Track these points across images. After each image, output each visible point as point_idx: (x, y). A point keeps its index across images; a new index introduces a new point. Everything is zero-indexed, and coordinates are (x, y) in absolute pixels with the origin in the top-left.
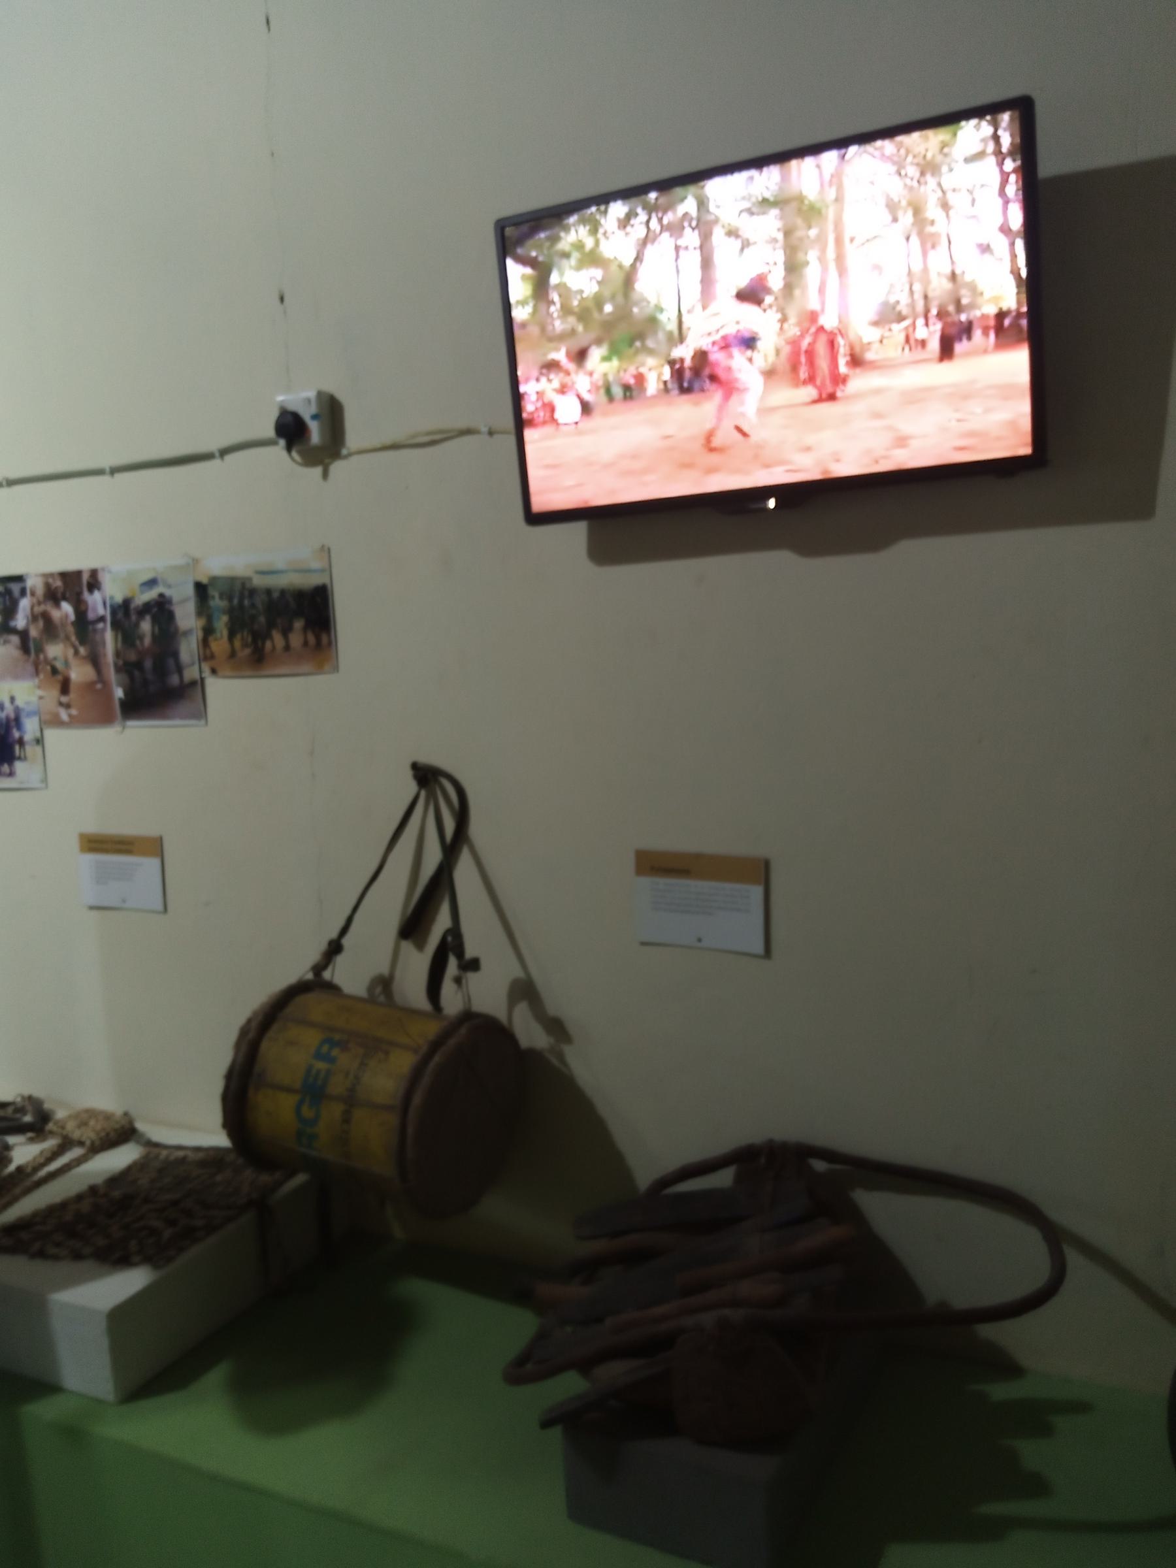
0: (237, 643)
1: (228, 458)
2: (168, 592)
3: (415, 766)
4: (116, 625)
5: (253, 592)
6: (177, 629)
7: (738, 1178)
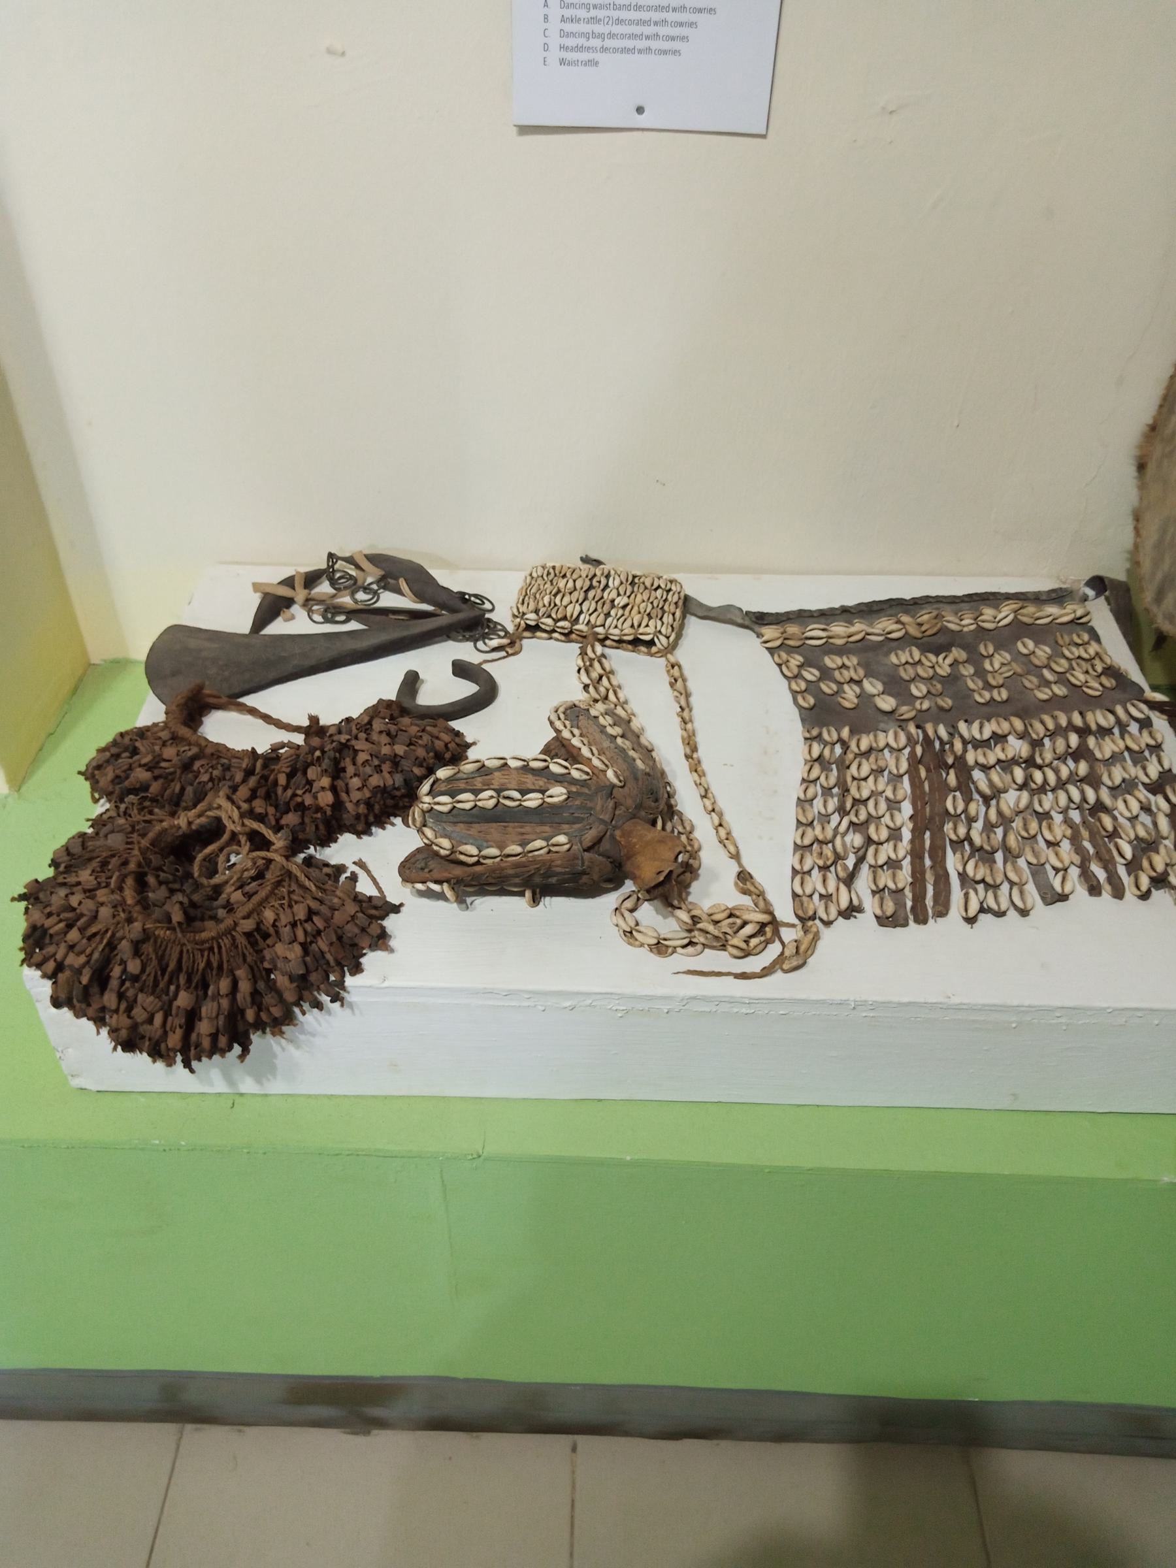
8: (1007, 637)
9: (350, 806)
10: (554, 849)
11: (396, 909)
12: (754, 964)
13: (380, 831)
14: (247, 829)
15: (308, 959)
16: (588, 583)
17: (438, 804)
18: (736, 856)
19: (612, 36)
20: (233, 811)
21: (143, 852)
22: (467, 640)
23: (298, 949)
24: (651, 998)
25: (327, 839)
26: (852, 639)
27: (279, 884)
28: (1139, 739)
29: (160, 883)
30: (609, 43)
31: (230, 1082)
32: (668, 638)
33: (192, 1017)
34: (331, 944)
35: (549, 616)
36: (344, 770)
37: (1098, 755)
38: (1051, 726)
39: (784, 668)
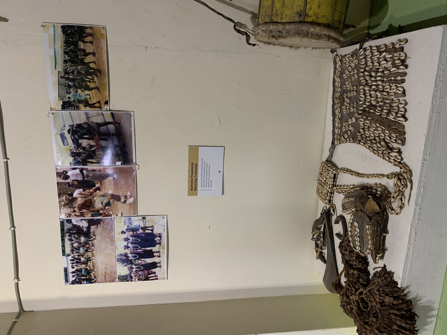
0: (92, 85)
1: (15, 226)
2: (67, 128)
4: (84, 162)
5: (66, 73)
6: (86, 123)
8: (343, 83)
9: (360, 266)
10: (369, 229)
11: (385, 266)
12: (409, 184)
13: (368, 260)
14: (358, 295)
15: (390, 295)
16: (320, 185)
17: (358, 249)
18: (383, 175)
19: (207, 178)
20: (353, 297)
21: (360, 320)
22: (332, 216)
23: (386, 297)
24: (415, 213)
25: (368, 273)
26: (339, 122)
27: (371, 294)
28: (368, 53)
29: (368, 319)
30: (208, 178)
31: (433, 316)
32: (334, 170)
33: (400, 326)
34: (387, 288)
35: (327, 197)
36: (352, 264)
37: (371, 67)
38: (363, 78)
39: (344, 142)
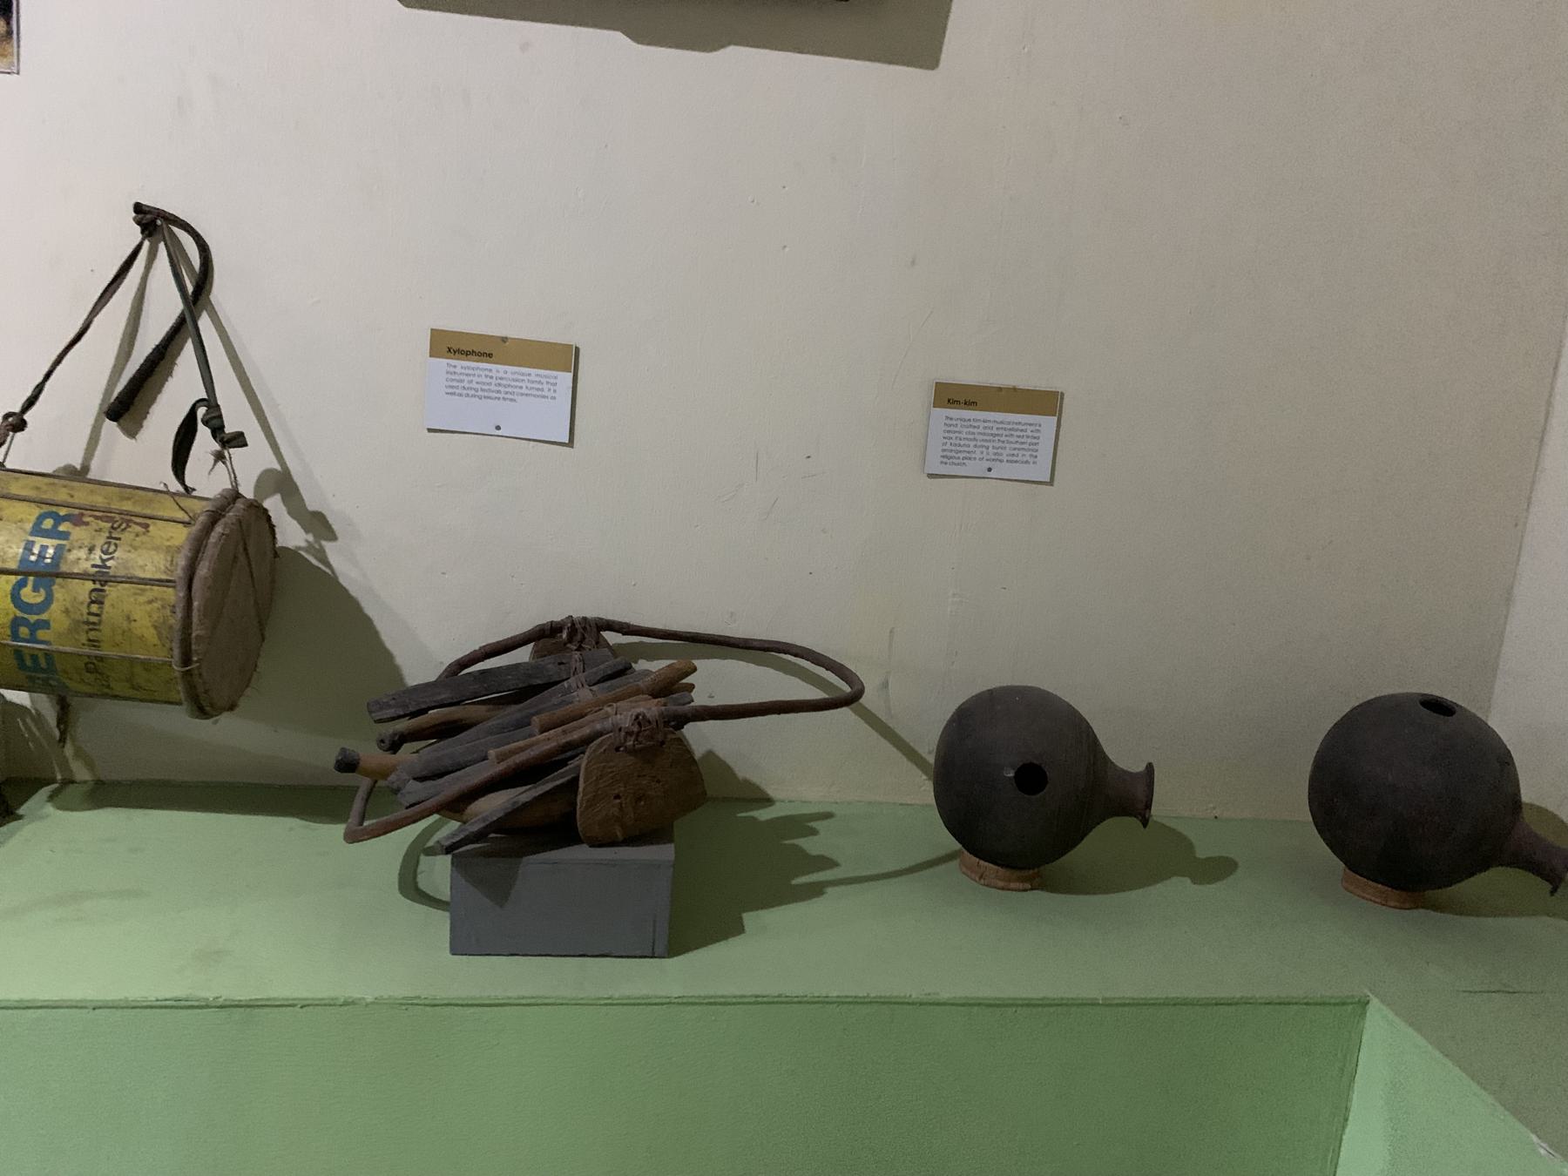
3: (138, 208)
7: (537, 653)
